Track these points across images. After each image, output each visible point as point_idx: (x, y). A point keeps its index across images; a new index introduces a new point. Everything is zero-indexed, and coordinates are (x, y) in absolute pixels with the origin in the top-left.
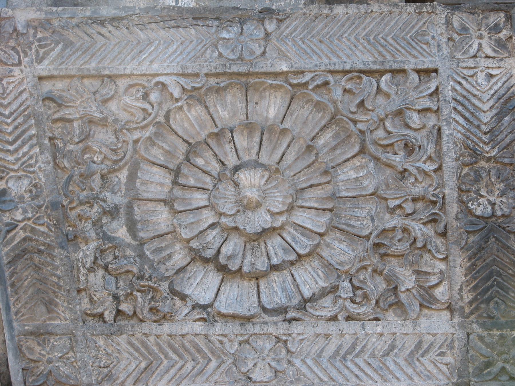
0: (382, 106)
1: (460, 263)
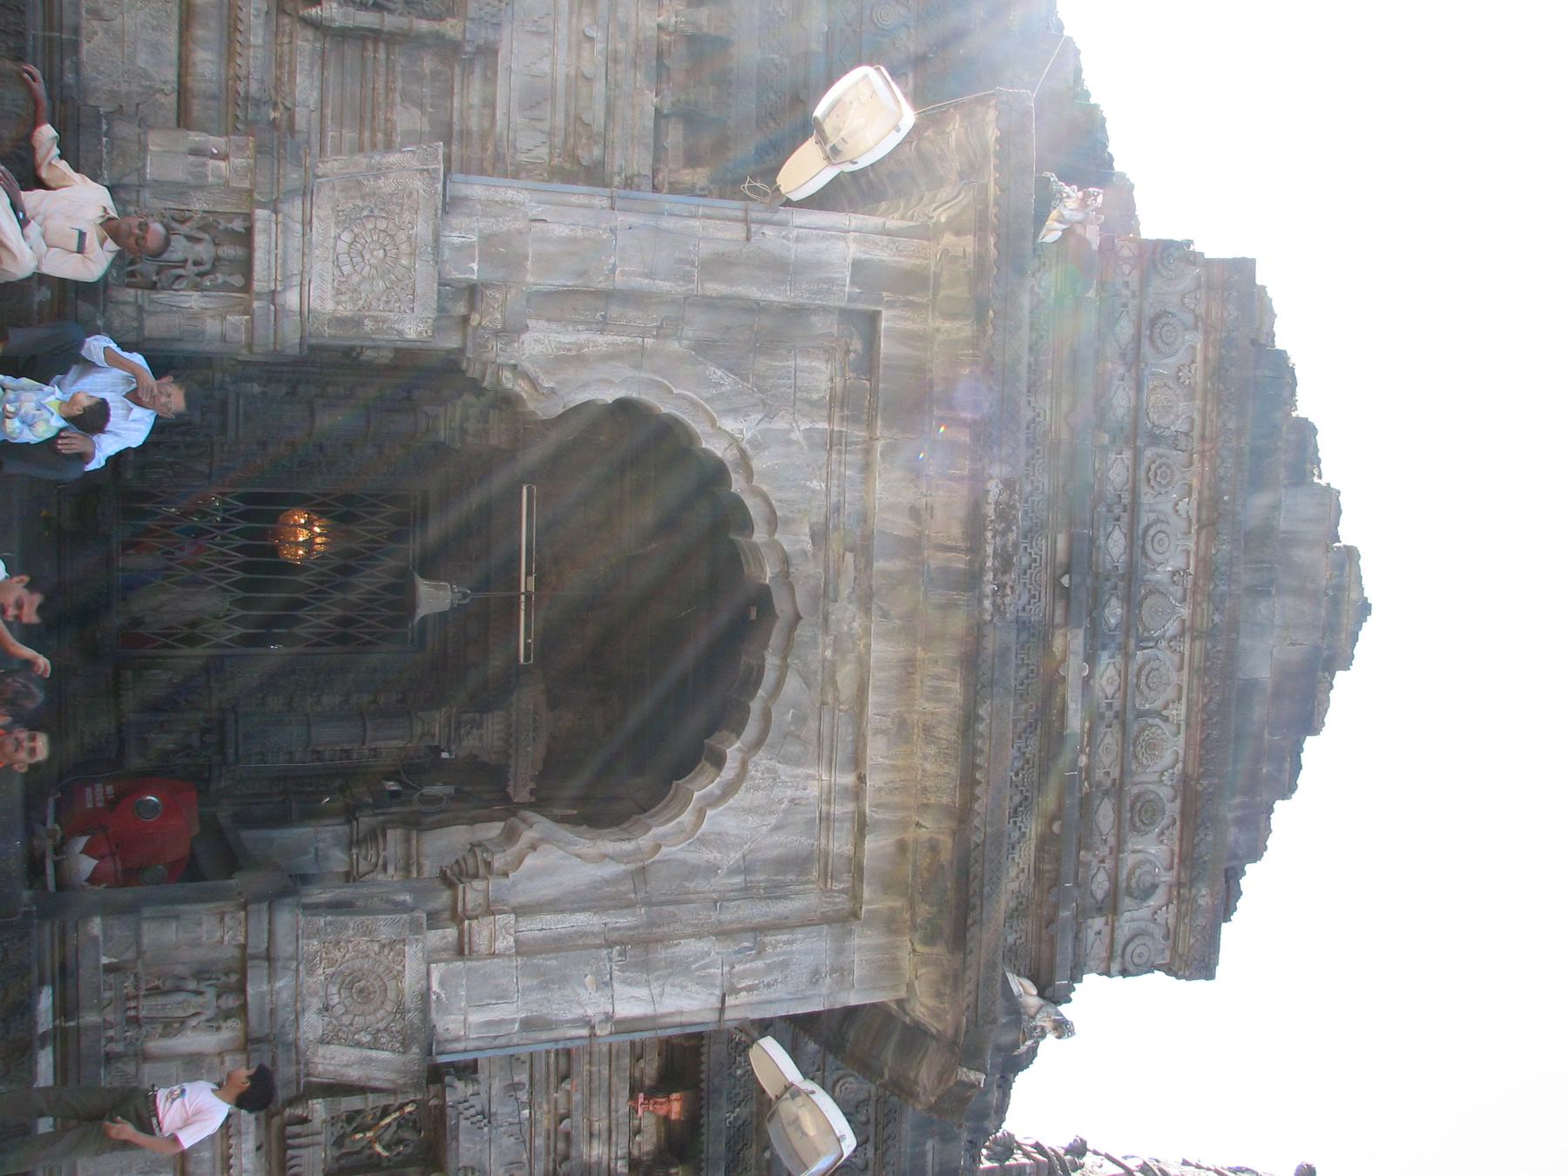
0: (402, 296)
1: (349, 314)
